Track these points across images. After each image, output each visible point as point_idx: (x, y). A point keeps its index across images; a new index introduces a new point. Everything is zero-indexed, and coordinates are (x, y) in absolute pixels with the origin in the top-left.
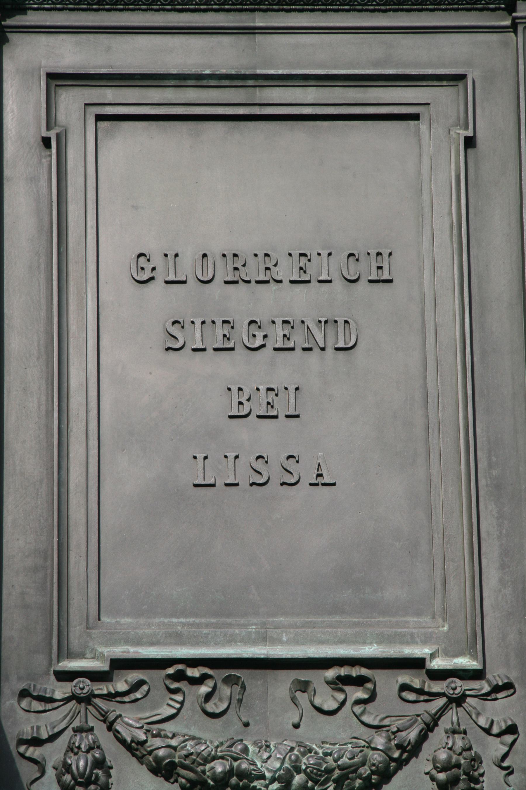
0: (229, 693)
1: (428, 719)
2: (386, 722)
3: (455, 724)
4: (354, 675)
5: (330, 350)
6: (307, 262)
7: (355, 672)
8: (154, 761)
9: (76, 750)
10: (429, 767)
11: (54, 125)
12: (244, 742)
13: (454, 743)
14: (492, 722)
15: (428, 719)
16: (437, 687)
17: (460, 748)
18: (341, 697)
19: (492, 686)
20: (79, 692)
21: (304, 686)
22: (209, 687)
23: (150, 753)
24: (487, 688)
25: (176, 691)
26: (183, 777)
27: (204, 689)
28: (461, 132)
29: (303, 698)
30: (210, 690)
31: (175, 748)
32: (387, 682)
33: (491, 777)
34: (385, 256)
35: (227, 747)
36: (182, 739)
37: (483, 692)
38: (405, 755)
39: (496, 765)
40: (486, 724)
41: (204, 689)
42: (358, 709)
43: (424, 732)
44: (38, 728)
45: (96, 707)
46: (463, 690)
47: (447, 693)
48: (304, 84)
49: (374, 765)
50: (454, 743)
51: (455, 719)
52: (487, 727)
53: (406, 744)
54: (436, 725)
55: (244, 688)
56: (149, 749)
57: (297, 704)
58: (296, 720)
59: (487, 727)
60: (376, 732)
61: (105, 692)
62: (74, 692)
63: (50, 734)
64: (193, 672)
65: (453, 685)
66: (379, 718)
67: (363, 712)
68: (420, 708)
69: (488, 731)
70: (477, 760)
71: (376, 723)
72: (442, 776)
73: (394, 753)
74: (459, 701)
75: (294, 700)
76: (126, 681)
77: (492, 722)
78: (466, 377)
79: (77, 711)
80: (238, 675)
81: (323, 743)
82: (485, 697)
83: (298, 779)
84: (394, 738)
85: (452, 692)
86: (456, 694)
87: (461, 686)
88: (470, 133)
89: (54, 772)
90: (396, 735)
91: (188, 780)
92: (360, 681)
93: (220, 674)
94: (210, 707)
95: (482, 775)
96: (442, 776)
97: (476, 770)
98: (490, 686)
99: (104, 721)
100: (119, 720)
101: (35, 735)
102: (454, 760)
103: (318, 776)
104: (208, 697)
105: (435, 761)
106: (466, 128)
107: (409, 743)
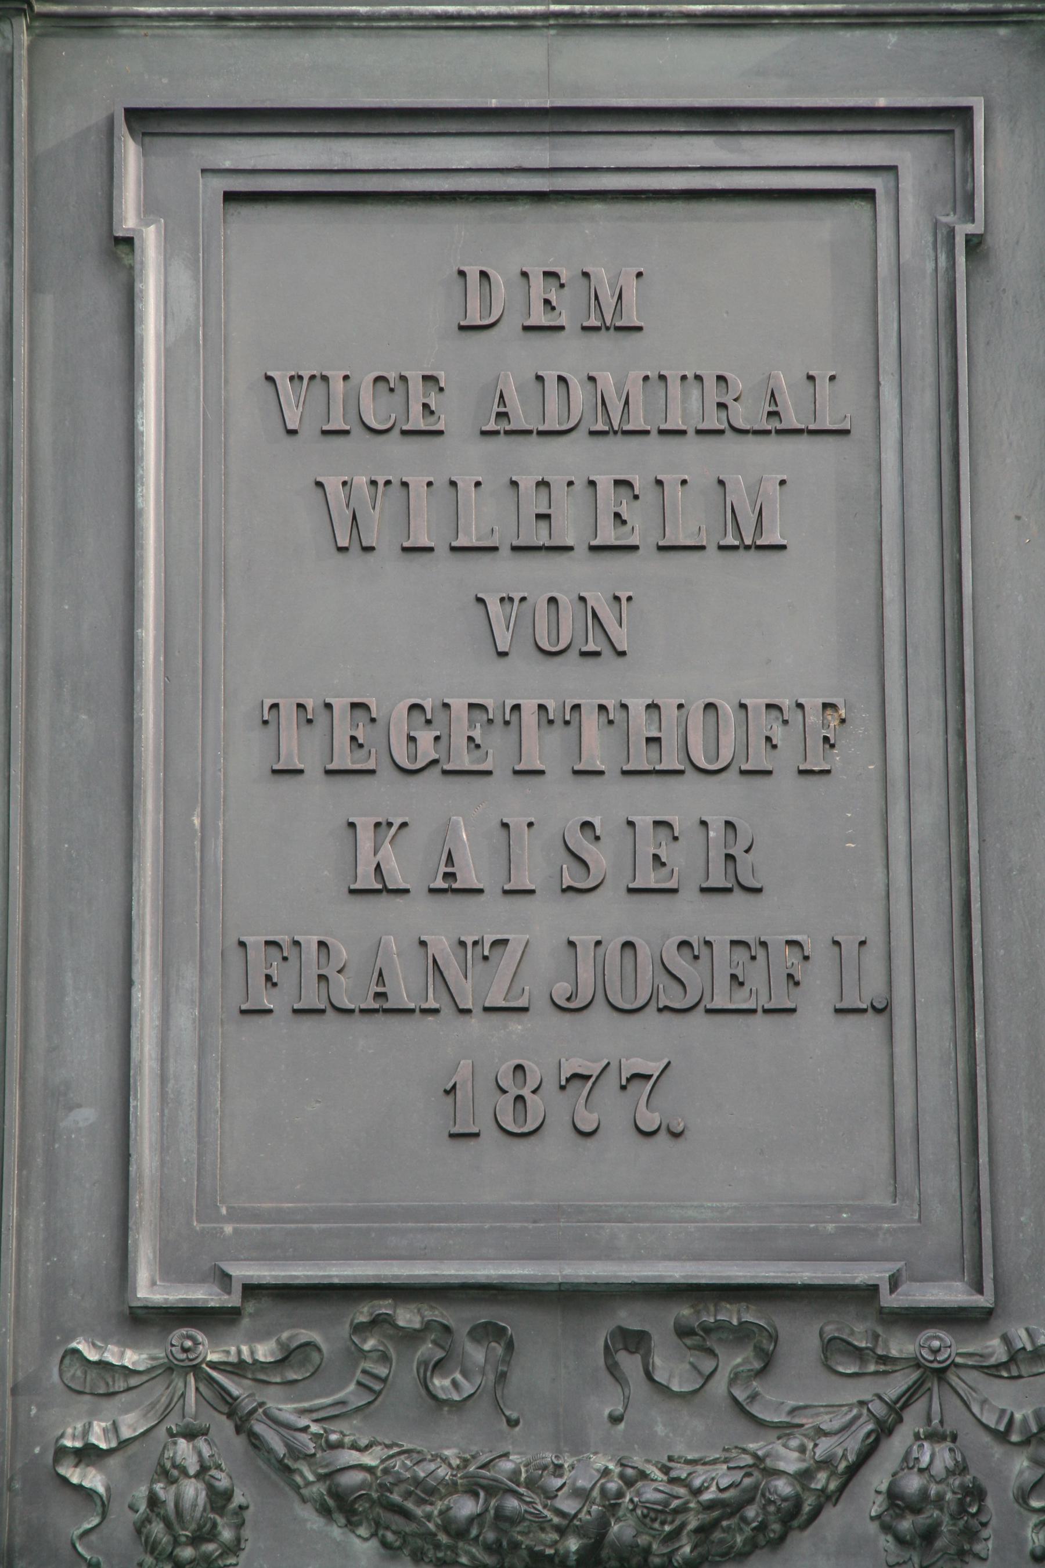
1: (878, 1408)
3: (936, 1422)
8: (530, 1557)
12: (511, 1457)
15: (878, 1408)
16: (900, 1345)
21: (635, 1341)
24: (1000, 1354)
27: (427, 1349)
29: (630, 1363)
32: (801, 1335)
37: (992, 1361)
40: (998, 1422)
45: (212, 1380)
46: (953, 1355)
48: (720, 129)
55: (510, 1346)
57: (617, 1375)
59: (1002, 1428)
60: (779, 1438)
62: (171, 1358)
65: (936, 1344)
67: (754, 1397)
68: (864, 1390)
69: (1002, 1436)
70: (976, 1493)
74: (935, 1374)
75: (613, 1369)
82: (993, 1371)
86: (940, 1362)
92: (742, 1334)
93: (459, 1318)
94: (440, 1384)
99: (230, 1415)
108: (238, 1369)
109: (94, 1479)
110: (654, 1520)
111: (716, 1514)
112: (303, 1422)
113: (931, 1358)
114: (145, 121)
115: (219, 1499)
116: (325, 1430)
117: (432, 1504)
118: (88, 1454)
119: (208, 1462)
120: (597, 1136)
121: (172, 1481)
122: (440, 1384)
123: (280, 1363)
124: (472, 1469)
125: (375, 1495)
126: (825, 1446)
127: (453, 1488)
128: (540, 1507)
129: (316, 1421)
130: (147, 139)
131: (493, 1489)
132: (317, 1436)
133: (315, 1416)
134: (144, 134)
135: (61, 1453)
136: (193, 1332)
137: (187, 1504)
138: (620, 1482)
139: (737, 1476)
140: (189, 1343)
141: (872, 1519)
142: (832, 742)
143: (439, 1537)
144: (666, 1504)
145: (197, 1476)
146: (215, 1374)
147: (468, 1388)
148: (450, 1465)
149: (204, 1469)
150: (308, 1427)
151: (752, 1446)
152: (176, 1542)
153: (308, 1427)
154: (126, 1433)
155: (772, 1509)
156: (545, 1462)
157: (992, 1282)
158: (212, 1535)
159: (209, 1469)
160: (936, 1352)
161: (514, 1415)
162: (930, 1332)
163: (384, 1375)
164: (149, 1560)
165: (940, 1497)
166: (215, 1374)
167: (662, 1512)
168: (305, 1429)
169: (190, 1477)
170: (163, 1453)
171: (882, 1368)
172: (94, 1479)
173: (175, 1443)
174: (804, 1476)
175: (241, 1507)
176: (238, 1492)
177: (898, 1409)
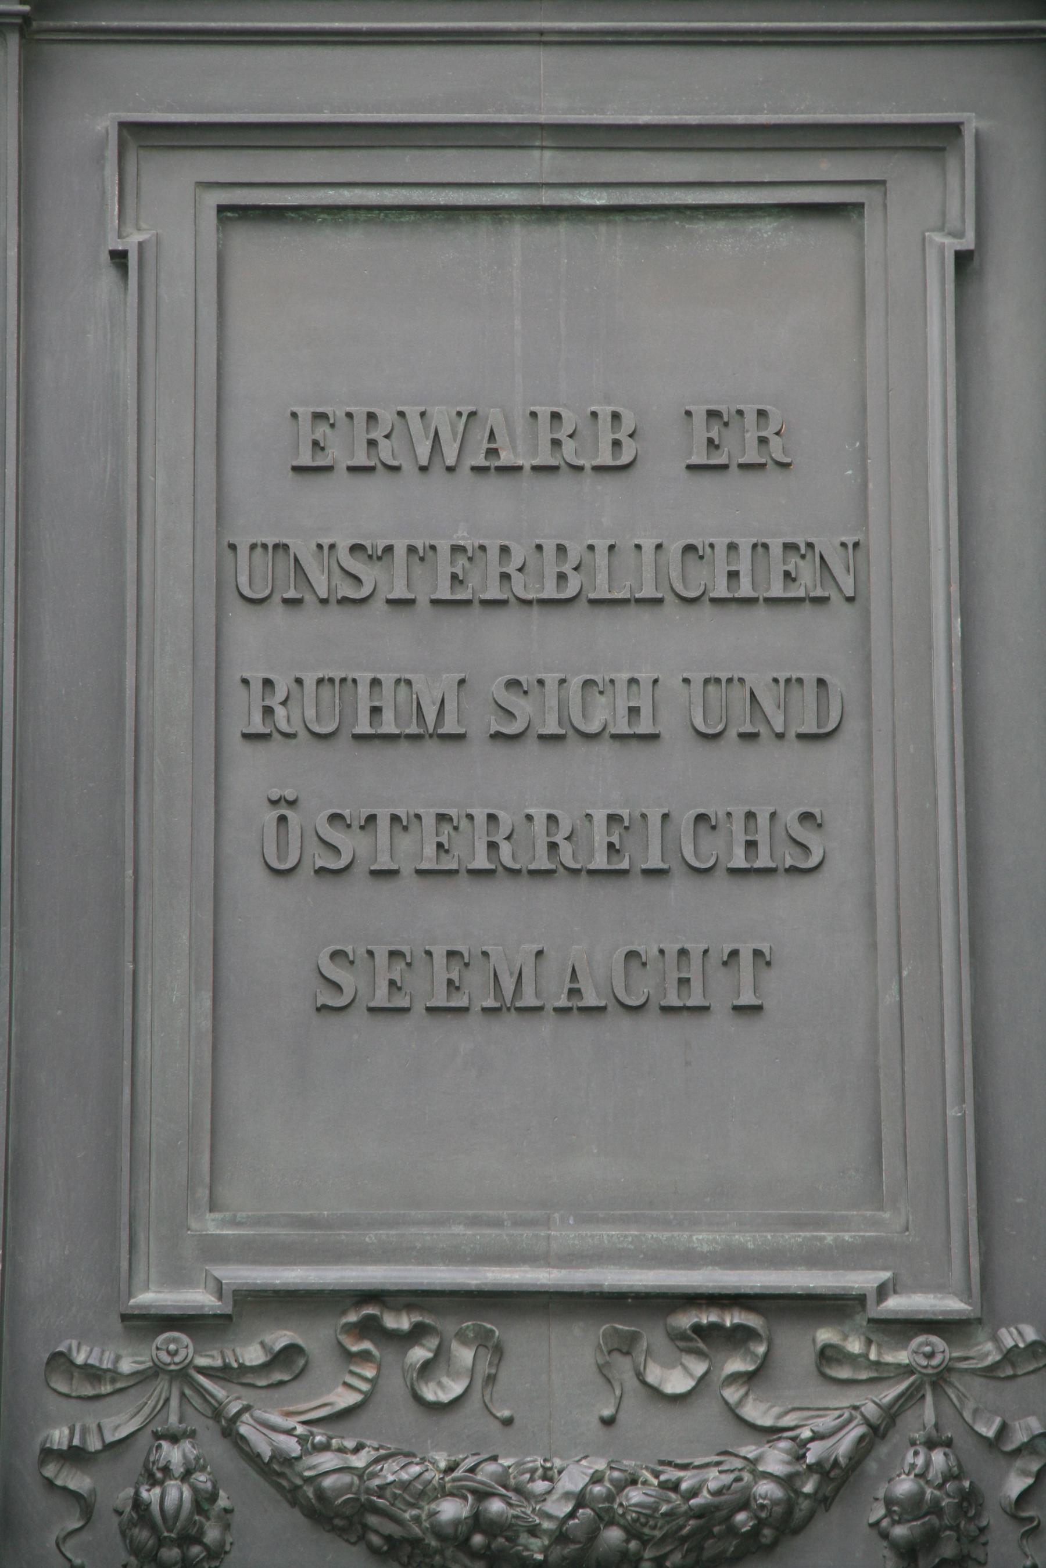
2: (788, 1421)
9: (159, 1475)
10: (879, 1511)
11: (143, 144)
12: (500, 1461)
17: (940, 1476)
18: (699, 1368)
19: (1005, 1351)
20: (167, 1359)
21: (626, 1345)
22: (430, 1350)
23: (309, 1480)
25: (365, 1356)
26: (376, 1532)
27: (419, 1354)
28: (947, 241)
30: (430, 1355)
31: (360, 1473)
33: (1002, 1540)
34: (763, 820)
35: (466, 1471)
36: (374, 1454)
38: (828, 1490)
42: (732, 1394)
43: (867, 1440)
44: (84, 1432)
45: (201, 1392)
47: (914, 1364)
49: (762, 1507)
50: (928, 1463)
53: (828, 1466)
56: (307, 1474)
58: (607, 1412)
61: (219, 1363)
62: (156, 1360)
64: (402, 1322)
66: (776, 1410)
71: (768, 1422)
72: (900, 1531)
73: (804, 1484)
76: (262, 1344)
79: (163, 1396)
80: (489, 1326)
85: (925, 1363)
86: (933, 1367)
87: (943, 1352)
88: (968, 242)
89: (115, 1520)
91: (388, 1538)
92: (740, 1337)
94: (430, 1393)
95: (982, 1530)
97: (971, 1519)
100: (246, 1417)
101: (76, 1442)
102: (928, 1496)
104: (426, 1369)
106: (960, 235)
107: (836, 1463)
108: (224, 1374)
109: (78, 1481)
110: (645, 1525)
112: (290, 1423)
113: (925, 1363)
114: (139, 135)
117: (421, 1508)
118: (75, 1456)
120: (825, 867)
121: (154, 1482)
127: (444, 1492)
129: (304, 1423)
130: (141, 152)
131: (482, 1495)
134: (141, 147)
135: (48, 1454)
136: (176, 1334)
143: (427, 1541)
150: (295, 1429)
151: (743, 1451)
152: (161, 1542)
153: (295, 1429)
154: (110, 1438)
158: (198, 1540)
160: (930, 1356)
161: (506, 1413)
162: (921, 1339)
164: (133, 1560)
165: (936, 1504)
167: (651, 1516)
168: (290, 1432)
172: (78, 1481)
173: (159, 1447)
174: (787, 1481)
175: (227, 1511)
177: (892, 1414)
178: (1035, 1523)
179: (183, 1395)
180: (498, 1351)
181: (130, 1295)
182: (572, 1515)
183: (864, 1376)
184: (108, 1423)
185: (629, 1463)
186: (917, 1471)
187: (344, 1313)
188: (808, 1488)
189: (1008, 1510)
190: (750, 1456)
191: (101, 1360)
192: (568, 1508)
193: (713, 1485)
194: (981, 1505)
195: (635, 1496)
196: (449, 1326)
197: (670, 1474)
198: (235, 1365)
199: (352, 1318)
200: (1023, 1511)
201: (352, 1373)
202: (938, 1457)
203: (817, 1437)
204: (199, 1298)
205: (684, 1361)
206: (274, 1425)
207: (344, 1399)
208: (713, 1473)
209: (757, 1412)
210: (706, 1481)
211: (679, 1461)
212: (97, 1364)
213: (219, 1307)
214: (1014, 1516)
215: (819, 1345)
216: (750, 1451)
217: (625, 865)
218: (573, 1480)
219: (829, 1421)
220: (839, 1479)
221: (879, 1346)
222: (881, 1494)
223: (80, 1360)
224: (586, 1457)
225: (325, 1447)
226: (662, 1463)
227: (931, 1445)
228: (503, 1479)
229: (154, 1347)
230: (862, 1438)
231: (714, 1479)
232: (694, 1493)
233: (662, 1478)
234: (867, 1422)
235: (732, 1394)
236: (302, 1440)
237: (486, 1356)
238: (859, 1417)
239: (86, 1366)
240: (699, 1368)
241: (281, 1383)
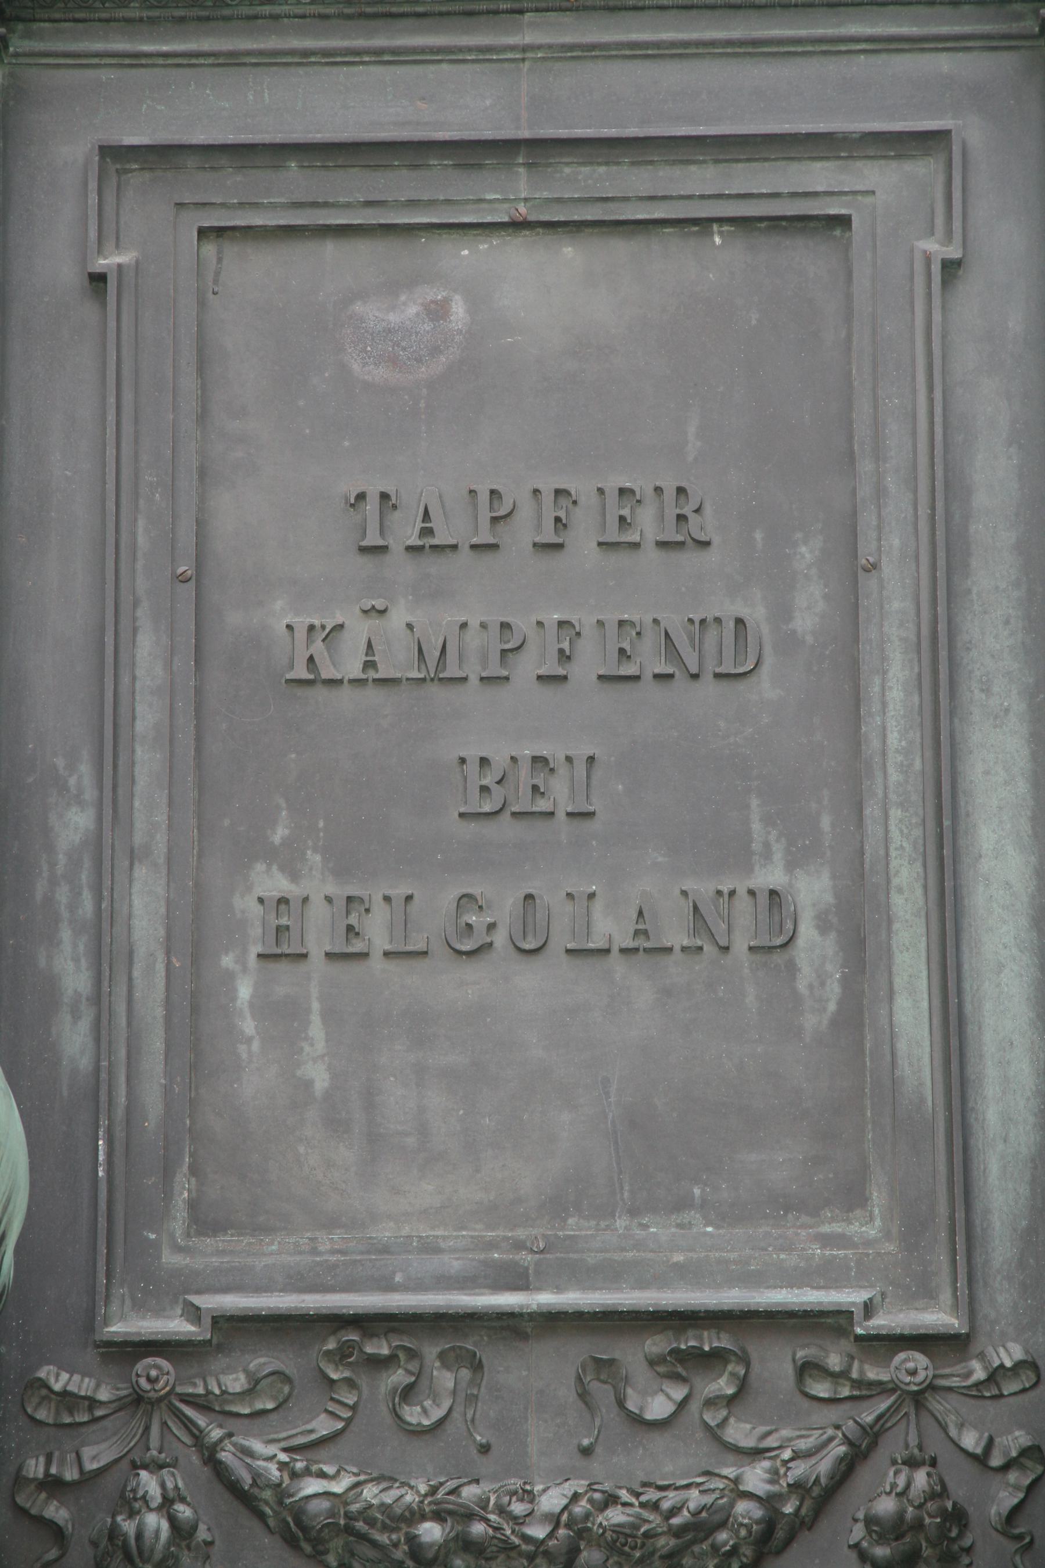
0: (451, 1385)
2: (771, 1442)
4: (698, 1341)
5: (708, 677)
6: (570, 505)
7: (709, 1341)
10: (858, 1532)
12: (481, 1485)
13: (908, 1486)
14: (990, 1442)
18: (678, 1393)
27: (399, 1377)
29: (602, 1392)
35: (448, 1494)
39: (997, 1530)
41: (399, 1377)
42: (712, 1418)
45: (187, 1424)
50: (908, 1486)
51: (913, 1440)
52: (979, 1451)
54: (874, 1444)
58: (586, 1442)
59: (979, 1451)
62: (136, 1386)
63: (69, 1388)
65: (911, 1365)
71: (749, 1443)
77: (990, 1442)
78: (104, 662)
81: (645, 1485)
83: (589, 1555)
84: (785, 1474)
87: (926, 1369)
89: (90, 1552)
90: (789, 1465)
94: (412, 1415)
96: (881, 1552)
98: (985, 1368)
103: (618, 1542)
104: (407, 1393)
105: (870, 1521)
107: (817, 1481)
111: (689, 1536)
113: (908, 1379)
115: (181, 1532)
116: (291, 1458)
118: (53, 1485)
119: (171, 1494)
121: (132, 1514)
122: (412, 1415)
123: (250, 1393)
124: (439, 1495)
125: (342, 1522)
126: (799, 1470)
128: (508, 1532)
129: (285, 1450)
131: (469, 1516)
132: (282, 1466)
133: (283, 1444)
137: (148, 1534)
138: (588, 1506)
139: (708, 1499)
140: (154, 1373)
141: (850, 1547)
142: (564, 521)
144: (635, 1527)
145: (159, 1509)
146: (189, 1411)
147: (437, 1414)
148: (418, 1492)
149: (167, 1502)
151: (725, 1472)
154: (90, 1466)
155: (743, 1532)
156: (513, 1487)
157: (108, 481)
159: (172, 1502)
160: (913, 1373)
163: (351, 1402)
166: (189, 1411)
169: (151, 1510)
170: (125, 1486)
171: (856, 1393)
172: (57, 1512)
174: (769, 1502)
176: (202, 1527)
178: (1027, 1540)
179: (164, 1424)
180: (478, 1367)
181: (106, 1324)
182: (551, 1535)
183: (845, 1392)
184: (87, 1452)
185: (607, 1486)
186: (899, 1489)
187: (324, 1341)
188: (788, 1509)
189: (999, 1527)
190: (731, 1476)
191: (80, 1387)
192: (548, 1529)
193: (692, 1505)
194: (965, 1526)
195: (615, 1516)
196: (431, 1351)
197: (651, 1495)
198: (217, 1391)
199: (331, 1345)
200: (1015, 1528)
201: (332, 1399)
202: (921, 1478)
203: (797, 1456)
204: (176, 1326)
205: (664, 1387)
206: (263, 1455)
207: (323, 1426)
208: (694, 1493)
209: (740, 1432)
210: (687, 1500)
211: (660, 1483)
212: (76, 1391)
213: (199, 1334)
214: (1004, 1534)
215: (800, 1363)
216: (730, 1472)
217: (635, 538)
218: (552, 1501)
219: (803, 1444)
220: (823, 1497)
221: (861, 1361)
222: (861, 1515)
223: (57, 1387)
224: (567, 1480)
225: (307, 1472)
226: (645, 1485)
227: (912, 1463)
228: (484, 1504)
229: (134, 1374)
230: (841, 1460)
231: (695, 1499)
232: (674, 1511)
233: (643, 1498)
234: (847, 1441)
235: (712, 1418)
236: (282, 1466)
237: (465, 1373)
238: (840, 1435)
239: (65, 1394)
240: (678, 1393)
241: (264, 1412)
